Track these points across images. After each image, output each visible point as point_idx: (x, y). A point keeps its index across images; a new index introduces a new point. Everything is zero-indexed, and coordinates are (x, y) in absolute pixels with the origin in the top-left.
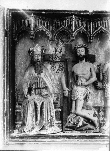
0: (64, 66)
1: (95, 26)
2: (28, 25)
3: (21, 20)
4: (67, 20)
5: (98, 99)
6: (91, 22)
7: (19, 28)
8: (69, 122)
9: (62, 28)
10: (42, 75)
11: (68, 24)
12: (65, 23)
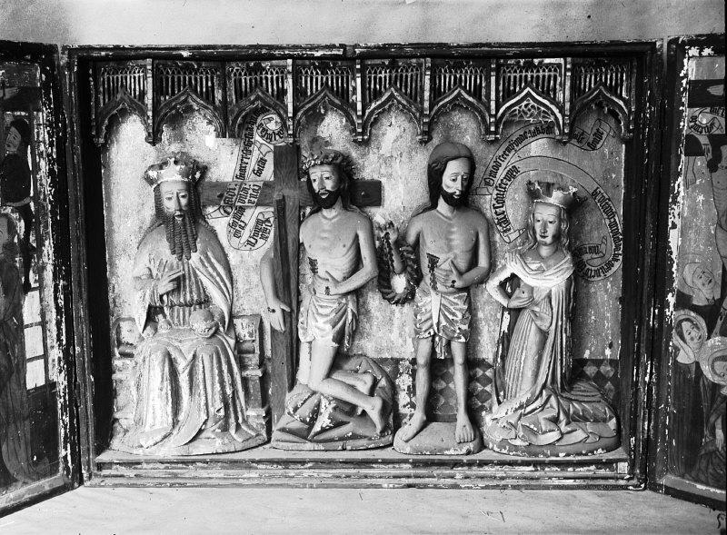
0: (272, 220)
1: (372, 86)
2: (137, 93)
3: (113, 74)
4: (272, 73)
5: (391, 331)
6: (359, 75)
7: (109, 100)
8: (289, 413)
9: (256, 99)
11: (275, 87)
12: (264, 82)
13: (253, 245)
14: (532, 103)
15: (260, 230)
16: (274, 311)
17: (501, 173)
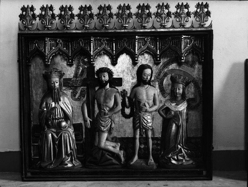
0: (86, 91)
10: (60, 103)
13: (80, 99)
15: (82, 95)
17: (162, 75)
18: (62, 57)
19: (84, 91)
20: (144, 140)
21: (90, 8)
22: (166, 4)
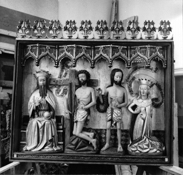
13: (62, 96)
14: (139, 57)
15: (65, 92)
16: (67, 113)
17: (131, 78)
18: (47, 60)
19: (67, 89)
20: (114, 132)
21: (90, 23)
22: (167, 21)
